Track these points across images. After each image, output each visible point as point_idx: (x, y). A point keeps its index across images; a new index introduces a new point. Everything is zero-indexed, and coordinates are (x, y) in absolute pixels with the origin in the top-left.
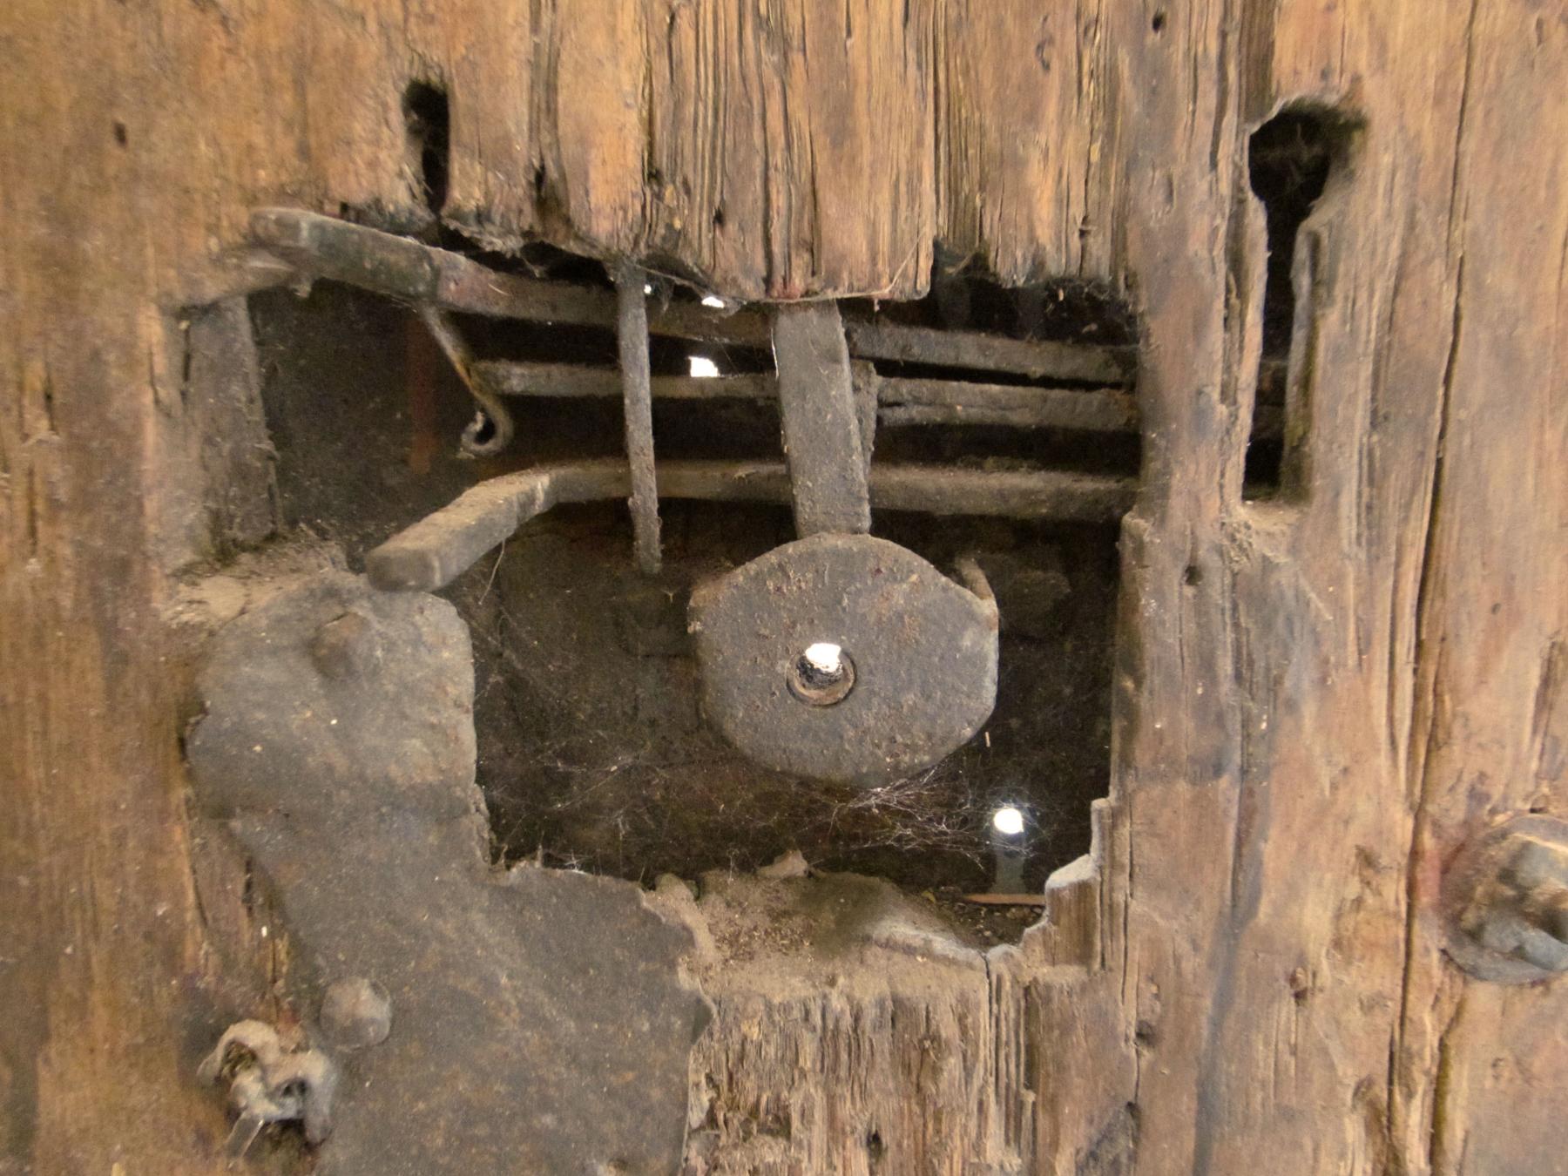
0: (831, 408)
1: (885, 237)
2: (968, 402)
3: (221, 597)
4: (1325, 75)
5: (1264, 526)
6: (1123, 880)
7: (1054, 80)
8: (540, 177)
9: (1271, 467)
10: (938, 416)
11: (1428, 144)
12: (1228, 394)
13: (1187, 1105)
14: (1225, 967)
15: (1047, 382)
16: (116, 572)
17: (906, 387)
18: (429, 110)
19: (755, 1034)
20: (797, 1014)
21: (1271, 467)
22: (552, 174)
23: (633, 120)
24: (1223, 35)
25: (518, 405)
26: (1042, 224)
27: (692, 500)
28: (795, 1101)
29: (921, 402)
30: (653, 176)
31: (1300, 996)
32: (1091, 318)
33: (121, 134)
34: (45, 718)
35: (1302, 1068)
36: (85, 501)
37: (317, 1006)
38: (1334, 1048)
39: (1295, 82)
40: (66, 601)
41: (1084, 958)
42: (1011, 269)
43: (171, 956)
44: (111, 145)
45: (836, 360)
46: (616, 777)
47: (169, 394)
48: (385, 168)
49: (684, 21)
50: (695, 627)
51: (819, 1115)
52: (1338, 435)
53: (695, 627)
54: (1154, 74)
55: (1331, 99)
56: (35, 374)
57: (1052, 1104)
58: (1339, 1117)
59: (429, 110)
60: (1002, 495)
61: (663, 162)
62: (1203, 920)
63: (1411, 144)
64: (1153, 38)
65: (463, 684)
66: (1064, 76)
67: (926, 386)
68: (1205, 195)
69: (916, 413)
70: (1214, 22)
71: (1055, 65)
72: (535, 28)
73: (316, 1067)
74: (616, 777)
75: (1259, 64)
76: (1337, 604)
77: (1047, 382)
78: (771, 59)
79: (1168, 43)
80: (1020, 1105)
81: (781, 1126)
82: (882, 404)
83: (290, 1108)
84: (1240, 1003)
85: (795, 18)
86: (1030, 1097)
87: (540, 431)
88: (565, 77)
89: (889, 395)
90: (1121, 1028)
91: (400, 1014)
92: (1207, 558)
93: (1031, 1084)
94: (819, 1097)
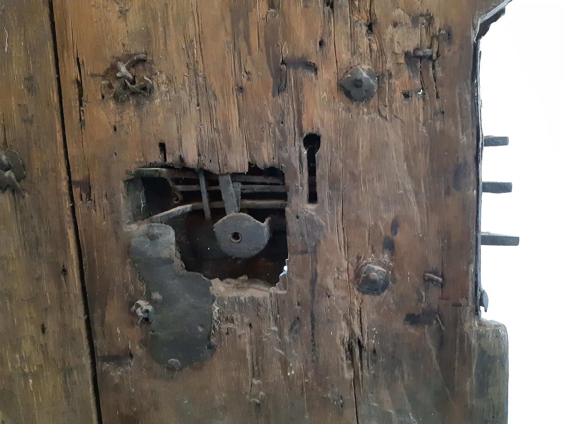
0: (231, 192)
1: (239, 162)
2: (257, 188)
3: (134, 227)
4: (313, 129)
5: (310, 207)
6: (291, 274)
7: (265, 134)
8: (181, 156)
9: (313, 198)
10: (252, 191)
11: (333, 138)
12: (302, 185)
13: (309, 318)
14: (313, 291)
15: (271, 184)
16: (117, 223)
17: (246, 187)
18: (162, 146)
19: (226, 303)
20: (233, 300)
21: (313, 198)
22: (182, 156)
23: (195, 147)
24: (294, 123)
25: (182, 193)
26: (266, 156)
27: (219, 208)
28: (234, 316)
29: (249, 189)
30: (199, 155)
31: (329, 297)
32: (274, 172)
33: (116, 154)
34: (106, 248)
35: (331, 311)
36: (112, 212)
37: (150, 297)
38: (337, 307)
39: (307, 130)
40: (110, 228)
41: (285, 289)
42: (261, 166)
43: (127, 289)
44: (114, 155)
45: (229, 183)
46: (201, 255)
47: (125, 195)
48: (156, 157)
49: (202, 129)
50: (214, 230)
51: (239, 320)
52: (323, 191)
53: (214, 230)
54: (282, 132)
55: (314, 133)
56: (104, 193)
57: (282, 317)
58: (340, 322)
59: (162, 146)
60: (271, 205)
61: (200, 152)
62: (308, 282)
63: (330, 138)
64: (282, 125)
65: (173, 240)
66: (267, 133)
67: (250, 186)
68: (296, 152)
69: (249, 191)
70: (292, 122)
71: (265, 131)
72: (178, 133)
73: (150, 308)
74: (201, 255)
75: (300, 127)
76: (325, 221)
77: (271, 184)
78: (216, 135)
79: (284, 126)
80: (277, 318)
81: (232, 321)
82: (242, 189)
83: (146, 316)
84: (316, 298)
85: (220, 128)
86: (278, 316)
87: (187, 198)
88: (183, 141)
89: (243, 188)
90: (294, 302)
91: (164, 298)
92: (299, 214)
93: (279, 313)
94: (239, 316)
